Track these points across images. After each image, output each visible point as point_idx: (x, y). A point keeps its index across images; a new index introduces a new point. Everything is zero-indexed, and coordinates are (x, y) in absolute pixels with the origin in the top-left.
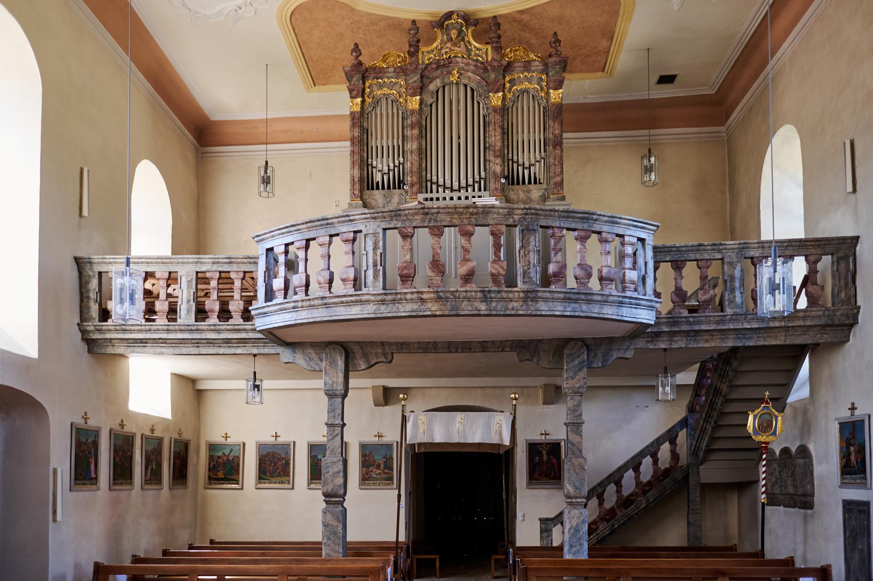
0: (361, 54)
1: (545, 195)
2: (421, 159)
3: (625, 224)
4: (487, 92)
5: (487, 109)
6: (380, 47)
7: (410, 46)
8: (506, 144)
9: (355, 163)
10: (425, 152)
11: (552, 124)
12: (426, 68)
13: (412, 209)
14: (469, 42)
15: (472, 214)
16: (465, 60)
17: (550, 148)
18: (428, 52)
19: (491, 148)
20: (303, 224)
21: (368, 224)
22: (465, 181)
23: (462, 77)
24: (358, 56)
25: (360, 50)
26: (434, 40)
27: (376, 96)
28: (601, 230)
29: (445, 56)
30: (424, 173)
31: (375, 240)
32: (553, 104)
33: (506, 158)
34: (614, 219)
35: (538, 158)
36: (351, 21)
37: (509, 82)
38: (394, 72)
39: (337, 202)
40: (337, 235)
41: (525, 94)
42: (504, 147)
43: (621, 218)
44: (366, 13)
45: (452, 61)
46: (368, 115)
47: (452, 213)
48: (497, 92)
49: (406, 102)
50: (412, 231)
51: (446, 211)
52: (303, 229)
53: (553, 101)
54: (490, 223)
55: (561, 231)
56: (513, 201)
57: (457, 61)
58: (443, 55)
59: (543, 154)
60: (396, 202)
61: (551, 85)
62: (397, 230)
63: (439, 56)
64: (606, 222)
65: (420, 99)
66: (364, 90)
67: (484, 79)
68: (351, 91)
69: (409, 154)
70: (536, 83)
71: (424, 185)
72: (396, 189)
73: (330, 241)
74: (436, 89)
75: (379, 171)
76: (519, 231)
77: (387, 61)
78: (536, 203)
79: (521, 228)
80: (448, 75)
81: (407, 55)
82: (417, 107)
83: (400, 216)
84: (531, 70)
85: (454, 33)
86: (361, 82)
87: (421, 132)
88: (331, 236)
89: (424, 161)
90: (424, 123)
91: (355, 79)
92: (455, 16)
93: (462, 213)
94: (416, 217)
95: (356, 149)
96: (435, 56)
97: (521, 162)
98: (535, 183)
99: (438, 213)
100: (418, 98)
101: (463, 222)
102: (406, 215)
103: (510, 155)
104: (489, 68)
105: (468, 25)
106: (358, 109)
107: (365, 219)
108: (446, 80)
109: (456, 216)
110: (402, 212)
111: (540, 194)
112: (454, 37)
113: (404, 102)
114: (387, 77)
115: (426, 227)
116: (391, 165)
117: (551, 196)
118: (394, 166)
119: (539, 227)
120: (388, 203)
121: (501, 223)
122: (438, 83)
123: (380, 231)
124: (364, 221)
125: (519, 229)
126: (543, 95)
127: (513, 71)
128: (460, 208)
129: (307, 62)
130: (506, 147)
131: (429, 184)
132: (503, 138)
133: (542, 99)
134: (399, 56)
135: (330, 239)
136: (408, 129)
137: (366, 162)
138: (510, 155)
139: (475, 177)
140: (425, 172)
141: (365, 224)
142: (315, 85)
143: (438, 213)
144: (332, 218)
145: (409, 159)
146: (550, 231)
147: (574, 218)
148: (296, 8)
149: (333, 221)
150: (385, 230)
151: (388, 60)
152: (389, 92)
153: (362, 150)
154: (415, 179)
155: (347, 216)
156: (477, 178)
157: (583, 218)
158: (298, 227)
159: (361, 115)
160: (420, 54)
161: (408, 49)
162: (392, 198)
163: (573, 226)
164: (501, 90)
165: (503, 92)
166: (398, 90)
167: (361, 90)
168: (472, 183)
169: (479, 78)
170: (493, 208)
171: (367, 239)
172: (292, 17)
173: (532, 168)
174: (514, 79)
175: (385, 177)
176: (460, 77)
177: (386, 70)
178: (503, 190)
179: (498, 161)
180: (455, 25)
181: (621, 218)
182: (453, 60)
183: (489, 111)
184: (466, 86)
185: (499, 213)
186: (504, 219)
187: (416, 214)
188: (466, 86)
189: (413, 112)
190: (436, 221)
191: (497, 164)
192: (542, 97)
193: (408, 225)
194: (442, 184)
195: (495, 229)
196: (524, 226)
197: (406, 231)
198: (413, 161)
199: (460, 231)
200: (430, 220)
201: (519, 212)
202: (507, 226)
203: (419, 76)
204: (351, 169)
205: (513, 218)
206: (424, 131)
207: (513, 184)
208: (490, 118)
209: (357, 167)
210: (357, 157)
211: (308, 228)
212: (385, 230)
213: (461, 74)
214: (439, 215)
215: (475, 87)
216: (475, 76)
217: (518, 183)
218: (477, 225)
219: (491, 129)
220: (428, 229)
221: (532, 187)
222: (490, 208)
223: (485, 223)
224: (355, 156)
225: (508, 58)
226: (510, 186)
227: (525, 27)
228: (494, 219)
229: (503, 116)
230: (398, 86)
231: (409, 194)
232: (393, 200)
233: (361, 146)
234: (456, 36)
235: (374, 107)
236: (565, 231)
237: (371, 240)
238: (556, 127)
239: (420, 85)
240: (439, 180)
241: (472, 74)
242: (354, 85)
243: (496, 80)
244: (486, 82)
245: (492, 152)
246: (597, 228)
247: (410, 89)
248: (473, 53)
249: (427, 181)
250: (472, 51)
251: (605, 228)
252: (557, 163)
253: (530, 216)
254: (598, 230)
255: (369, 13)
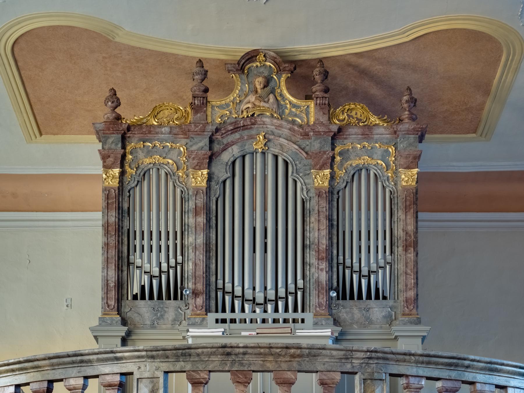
0: (119, 104)
1: (391, 316)
2: (208, 258)
3: (508, 372)
4: (308, 167)
5: (308, 191)
6: (145, 90)
7: (194, 97)
8: (335, 241)
9: (109, 261)
10: (214, 248)
11: (403, 217)
12: (217, 130)
13: (207, 348)
14: (281, 95)
15: (293, 356)
16: (275, 121)
17: (399, 250)
18: (221, 107)
19: (312, 246)
20: (44, 359)
21: (142, 365)
22: (274, 292)
23: (270, 144)
24: (116, 108)
25: (118, 99)
26: (231, 90)
27: (142, 166)
28: (475, 381)
29: (245, 114)
30: (213, 279)
31: (153, 387)
32: (404, 187)
33: (335, 261)
34: (493, 366)
35: (382, 263)
36: (104, 55)
37: (340, 154)
38: (170, 133)
39: (69, 301)
40: (97, 376)
41: (363, 172)
42: (332, 246)
43: (503, 364)
44: (128, 46)
45: (256, 121)
46: (129, 192)
47: (265, 355)
48: (321, 168)
49: (187, 176)
50: (207, 377)
51: (257, 351)
52: (44, 366)
53: (404, 184)
54: (319, 369)
55: (419, 381)
56: (345, 322)
57: (264, 122)
58: (242, 112)
59: (389, 258)
60: (170, 318)
61: (402, 161)
62: (185, 374)
63: (236, 113)
64: (482, 369)
65: (209, 174)
66: (124, 156)
67: (303, 149)
68: (104, 158)
69: (190, 251)
70: (380, 157)
71: (213, 295)
72: (170, 299)
73: (84, 384)
74: (232, 159)
75: (137, 267)
76: (360, 381)
77: (158, 117)
78: (378, 326)
79: (363, 377)
80: (251, 141)
81: (189, 109)
82: (204, 184)
83: (190, 355)
84: (372, 138)
85: (259, 82)
86: (120, 145)
87: (208, 220)
88: (86, 378)
89: (214, 261)
90: (214, 207)
91: (110, 140)
92: (261, 57)
93: (279, 355)
94: (213, 358)
95: (113, 241)
96: (231, 113)
97: (356, 267)
98: (377, 297)
99: (244, 354)
100: (205, 172)
101: (280, 366)
102: (198, 355)
103: (341, 258)
104: (312, 134)
105: (279, 71)
106: (115, 183)
107: (139, 357)
108: (248, 148)
109: (271, 358)
110: (192, 351)
111: (384, 314)
112: (259, 87)
113: (185, 176)
114: (158, 140)
115: (229, 371)
116: (164, 266)
117: (401, 318)
118: (169, 267)
119: (388, 375)
120: (158, 319)
121: (334, 369)
122: (235, 151)
123: (161, 375)
124: (137, 360)
125: (360, 378)
126: (390, 175)
127: (346, 139)
128: (277, 348)
129: (32, 104)
130: (335, 246)
131: (220, 294)
132: (330, 233)
133: (388, 180)
134: (177, 110)
135: (84, 382)
136: (191, 215)
137: (126, 260)
138: (341, 258)
139: (289, 286)
140: (214, 277)
141: (138, 364)
142: (41, 134)
143: (244, 354)
144: (89, 354)
145: (190, 257)
146: (402, 381)
147: (437, 364)
148: (22, 35)
149: (91, 357)
150: (166, 373)
151: (160, 115)
152: (162, 160)
153: (120, 242)
154: (200, 287)
155: (112, 352)
156: (291, 288)
157: (450, 365)
158: (36, 363)
159: (119, 192)
160: (209, 109)
161: (191, 101)
162: (165, 312)
163: (435, 374)
164: (329, 165)
165: (332, 168)
166: (175, 159)
167: (120, 156)
168: (284, 295)
169: (297, 147)
170: (324, 349)
171: (141, 385)
172: (16, 46)
173: (372, 277)
174: (348, 150)
175: (155, 282)
176: (268, 143)
177: (158, 130)
178: (330, 307)
179: (324, 265)
180: (262, 70)
181: (503, 364)
182: (258, 119)
183: (311, 195)
184: (276, 157)
185: (332, 357)
186: (339, 364)
187: (212, 354)
188: (276, 157)
189: (197, 192)
190: (242, 364)
191: (322, 270)
192: (388, 177)
193: (201, 368)
194: (240, 294)
195: (325, 377)
196: (366, 374)
197: (198, 377)
198: (198, 262)
199: (275, 379)
200: (233, 362)
201: (361, 355)
202: (342, 373)
203: (207, 141)
204: (103, 268)
205: (351, 363)
206: (214, 218)
207: (344, 298)
208: (311, 205)
209: (112, 267)
210: (113, 253)
211: (52, 365)
212: (166, 373)
213: (269, 140)
214: (247, 356)
215: (289, 159)
216: (290, 143)
217: (352, 298)
218: (299, 371)
219: (313, 219)
220: (229, 374)
221: (373, 303)
222: (320, 349)
223: (312, 368)
224: (110, 251)
225: (339, 120)
226: (341, 302)
227: (364, 73)
228: (324, 364)
229: (330, 202)
230: (175, 153)
231: (191, 307)
232: (166, 316)
233: (119, 236)
234: (262, 86)
235: (138, 181)
236: (423, 382)
237: (146, 386)
238: (408, 221)
239: (209, 153)
240: (235, 289)
241: (286, 141)
242: (110, 149)
243: (321, 153)
244: (307, 153)
245: (314, 253)
246: (469, 376)
247: (194, 159)
248: (287, 111)
249: (217, 289)
250: (286, 108)
251: (480, 377)
252: (409, 271)
253: (376, 361)
254: (471, 380)
255: (133, 47)
